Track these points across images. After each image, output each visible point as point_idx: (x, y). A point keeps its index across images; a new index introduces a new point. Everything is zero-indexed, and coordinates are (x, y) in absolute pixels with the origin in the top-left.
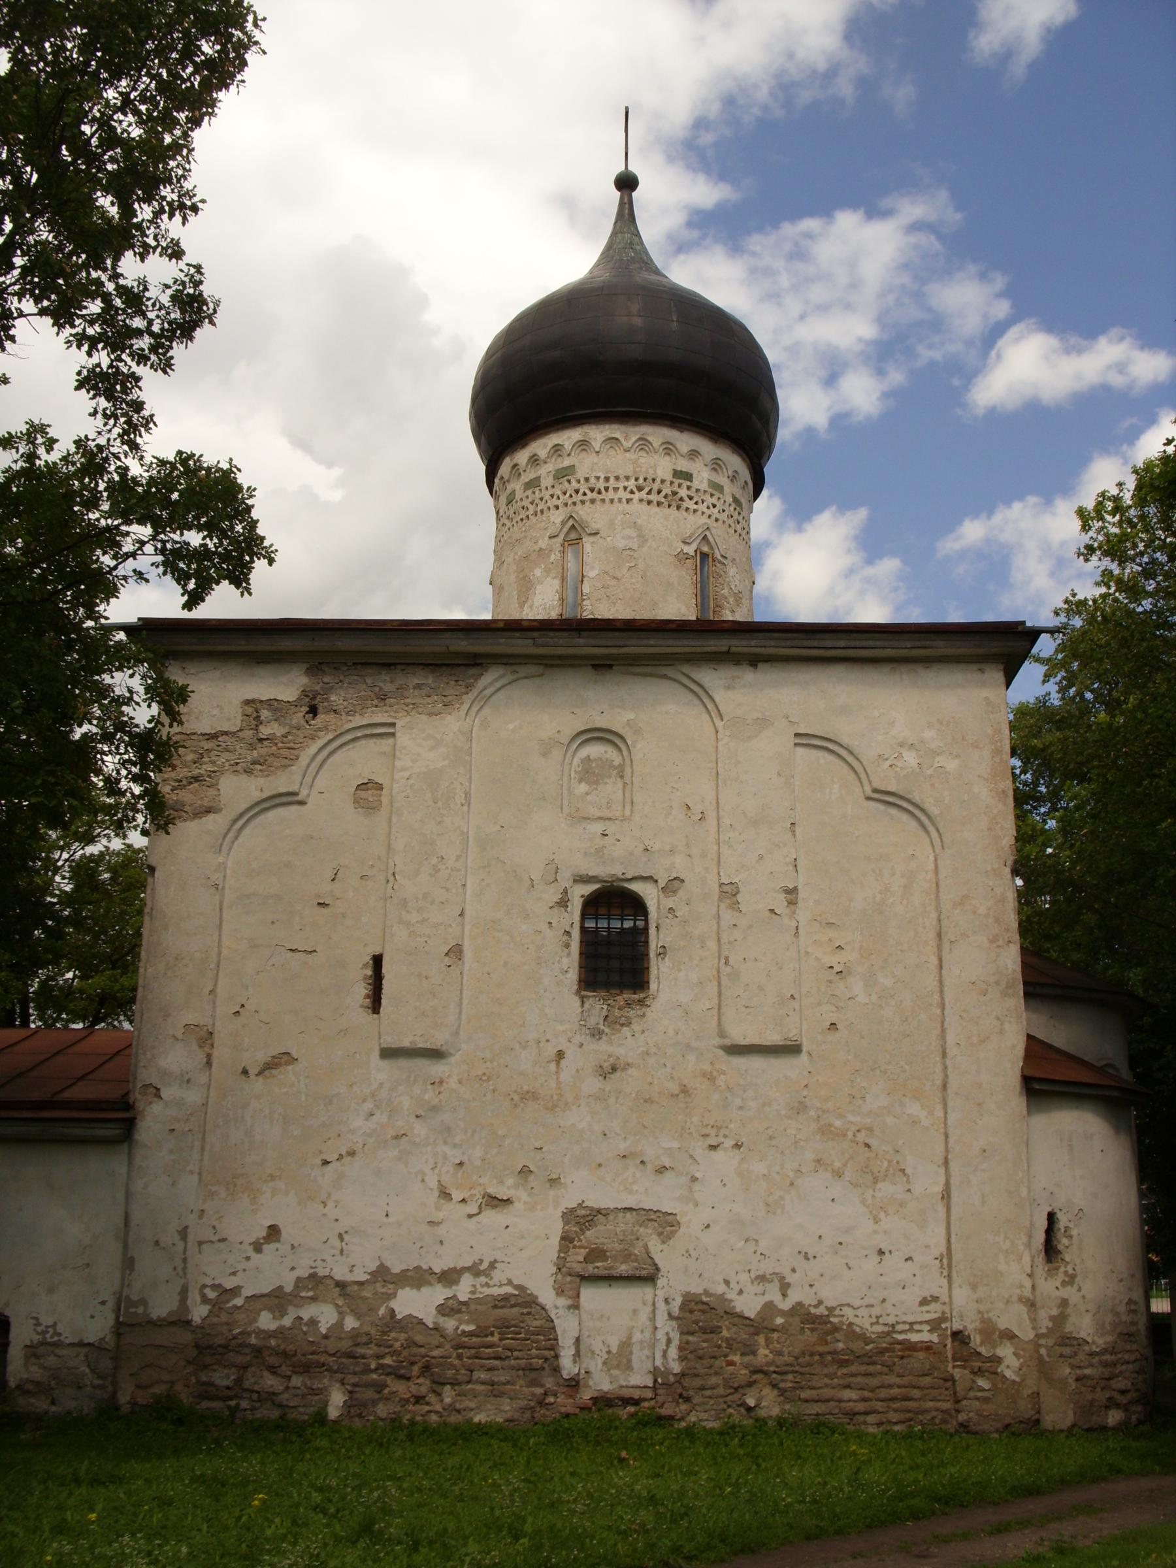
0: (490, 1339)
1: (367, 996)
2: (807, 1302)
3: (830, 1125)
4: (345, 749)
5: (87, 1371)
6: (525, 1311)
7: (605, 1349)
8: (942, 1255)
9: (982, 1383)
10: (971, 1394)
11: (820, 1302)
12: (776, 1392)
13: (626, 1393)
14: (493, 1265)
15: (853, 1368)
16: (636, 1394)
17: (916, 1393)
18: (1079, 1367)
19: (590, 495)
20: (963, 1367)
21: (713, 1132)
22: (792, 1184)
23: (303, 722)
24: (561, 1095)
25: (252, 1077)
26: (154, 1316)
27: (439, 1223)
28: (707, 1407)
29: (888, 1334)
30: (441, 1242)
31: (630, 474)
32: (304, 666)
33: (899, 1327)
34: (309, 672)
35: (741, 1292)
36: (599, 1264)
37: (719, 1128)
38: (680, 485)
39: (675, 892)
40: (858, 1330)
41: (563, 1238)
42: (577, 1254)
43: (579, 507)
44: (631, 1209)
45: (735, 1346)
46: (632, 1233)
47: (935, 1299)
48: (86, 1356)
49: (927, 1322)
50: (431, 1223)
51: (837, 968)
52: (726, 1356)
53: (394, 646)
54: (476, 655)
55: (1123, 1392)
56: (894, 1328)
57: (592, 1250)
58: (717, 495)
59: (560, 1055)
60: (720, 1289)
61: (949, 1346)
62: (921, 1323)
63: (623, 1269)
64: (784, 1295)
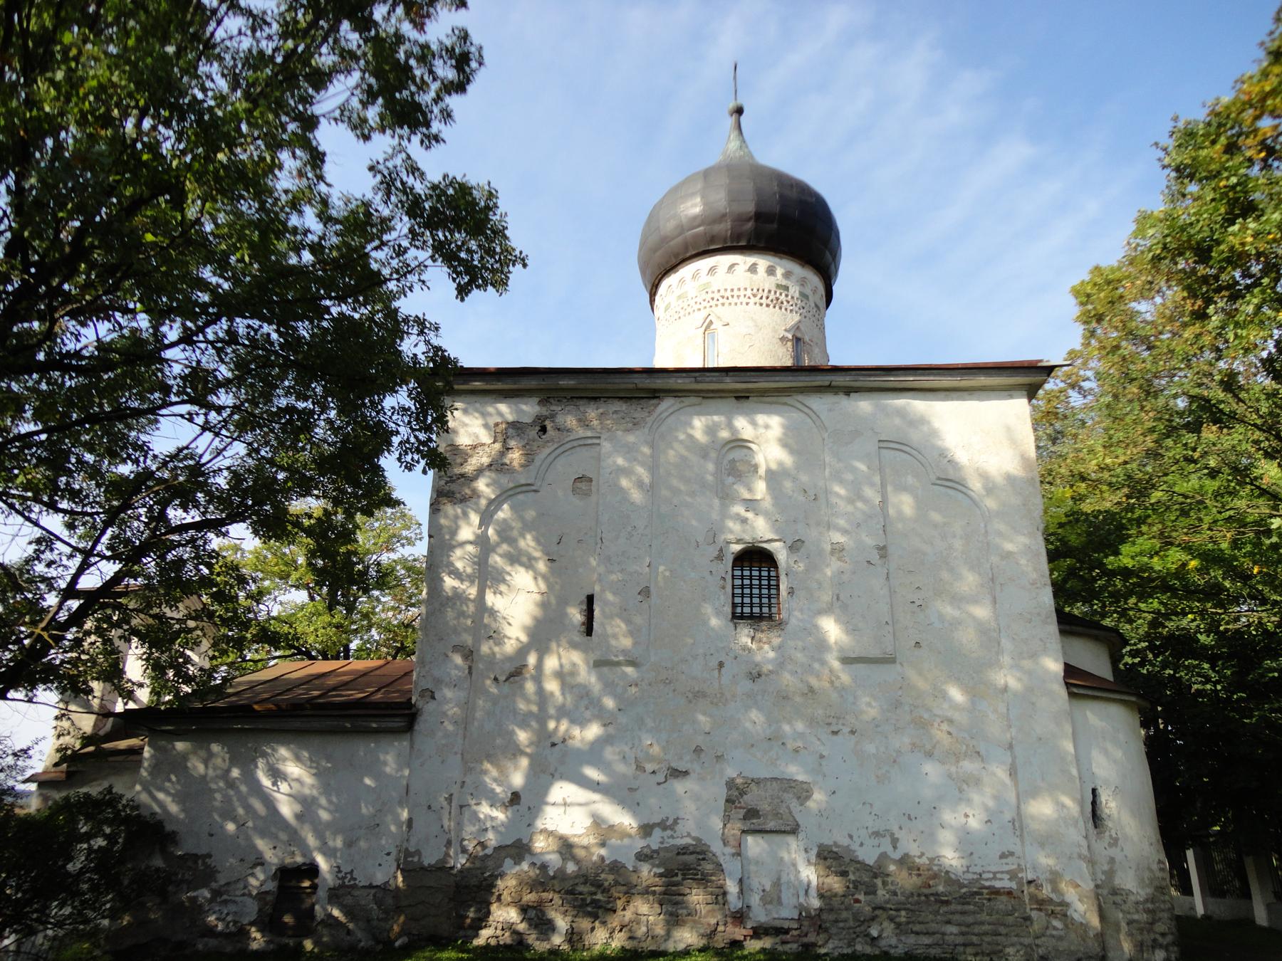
0: (675, 879)
1: (583, 624)
2: (912, 854)
3: (921, 717)
4: (567, 453)
5: (375, 907)
6: (701, 857)
7: (761, 888)
8: (1014, 820)
9: (1056, 923)
10: (1048, 932)
11: (923, 854)
12: (892, 925)
13: (778, 924)
14: (676, 821)
15: (953, 907)
16: (786, 925)
17: (1003, 930)
18: (1129, 913)
19: (721, 300)
20: (1040, 910)
21: (834, 721)
22: (895, 761)
23: (537, 437)
24: (722, 694)
25: (501, 683)
26: (426, 863)
27: (636, 790)
28: (842, 936)
29: (977, 880)
30: (638, 804)
31: (748, 286)
32: (537, 400)
33: (984, 876)
34: (542, 402)
35: (862, 845)
36: (755, 821)
37: (838, 718)
38: (781, 294)
39: (798, 550)
40: (953, 876)
41: (727, 801)
42: (738, 813)
43: (714, 309)
44: (776, 779)
45: (860, 887)
46: (778, 798)
47: (1012, 854)
48: (374, 896)
49: (1007, 872)
50: (630, 789)
51: (918, 603)
52: (853, 895)
53: (599, 384)
54: (655, 391)
55: (1163, 935)
56: (980, 875)
57: (749, 811)
58: (805, 301)
59: (721, 665)
60: (845, 841)
61: (1025, 892)
62: (1002, 872)
63: (771, 825)
64: (895, 847)
